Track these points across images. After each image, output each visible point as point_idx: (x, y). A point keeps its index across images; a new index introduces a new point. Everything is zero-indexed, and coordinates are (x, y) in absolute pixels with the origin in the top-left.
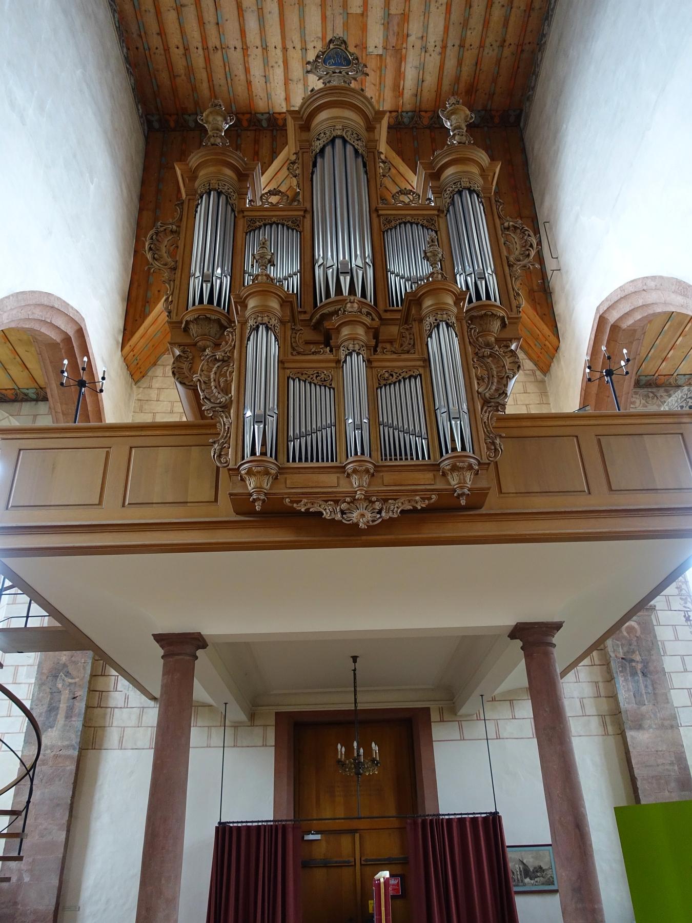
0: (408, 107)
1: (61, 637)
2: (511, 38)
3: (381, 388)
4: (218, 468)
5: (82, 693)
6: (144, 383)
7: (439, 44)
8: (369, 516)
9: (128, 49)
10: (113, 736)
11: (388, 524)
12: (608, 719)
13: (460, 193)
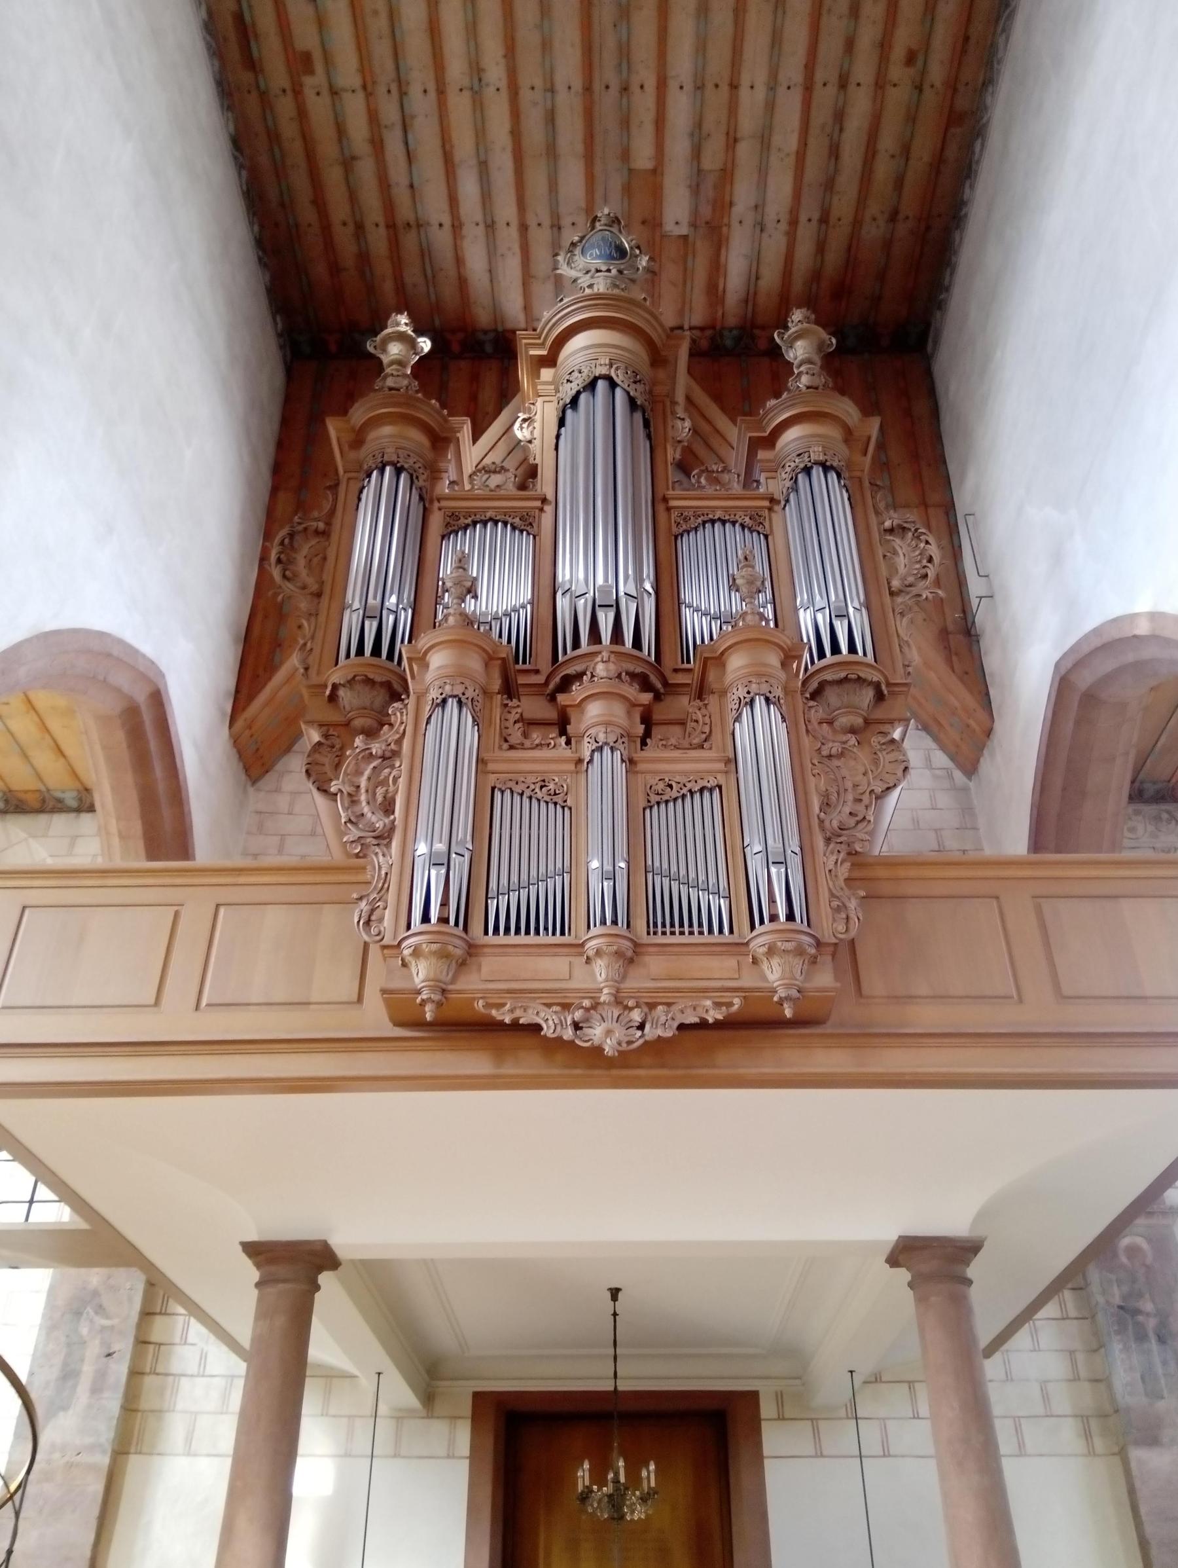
0: (732, 321)
1: (93, 1244)
2: (909, 207)
3: (651, 807)
4: (366, 945)
5: (124, 1346)
6: (269, 781)
7: (785, 218)
8: (619, 1033)
9: (262, 226)
10: (175, 1429)
11: (657, 1047)
12: (1094, 1424)
13: (807, 470)
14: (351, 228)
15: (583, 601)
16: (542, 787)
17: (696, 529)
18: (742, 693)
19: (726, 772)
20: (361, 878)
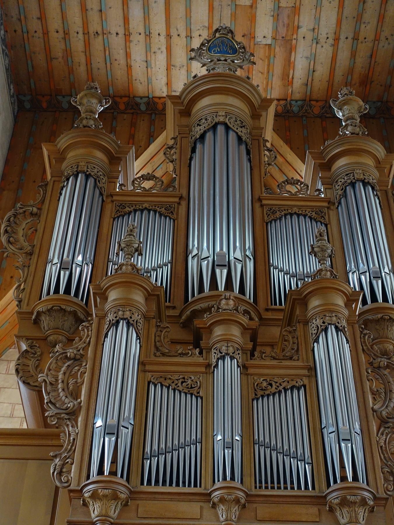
0: (297, 96)
3: (257, 399)
7: (331, 36)
13: (353, 185)
14: (61, 34)
15: (206, 262)
16: (182, 383)
17: (280, 219)
18: (319, 322)
19: (309, 376)
20: (54, 442)
